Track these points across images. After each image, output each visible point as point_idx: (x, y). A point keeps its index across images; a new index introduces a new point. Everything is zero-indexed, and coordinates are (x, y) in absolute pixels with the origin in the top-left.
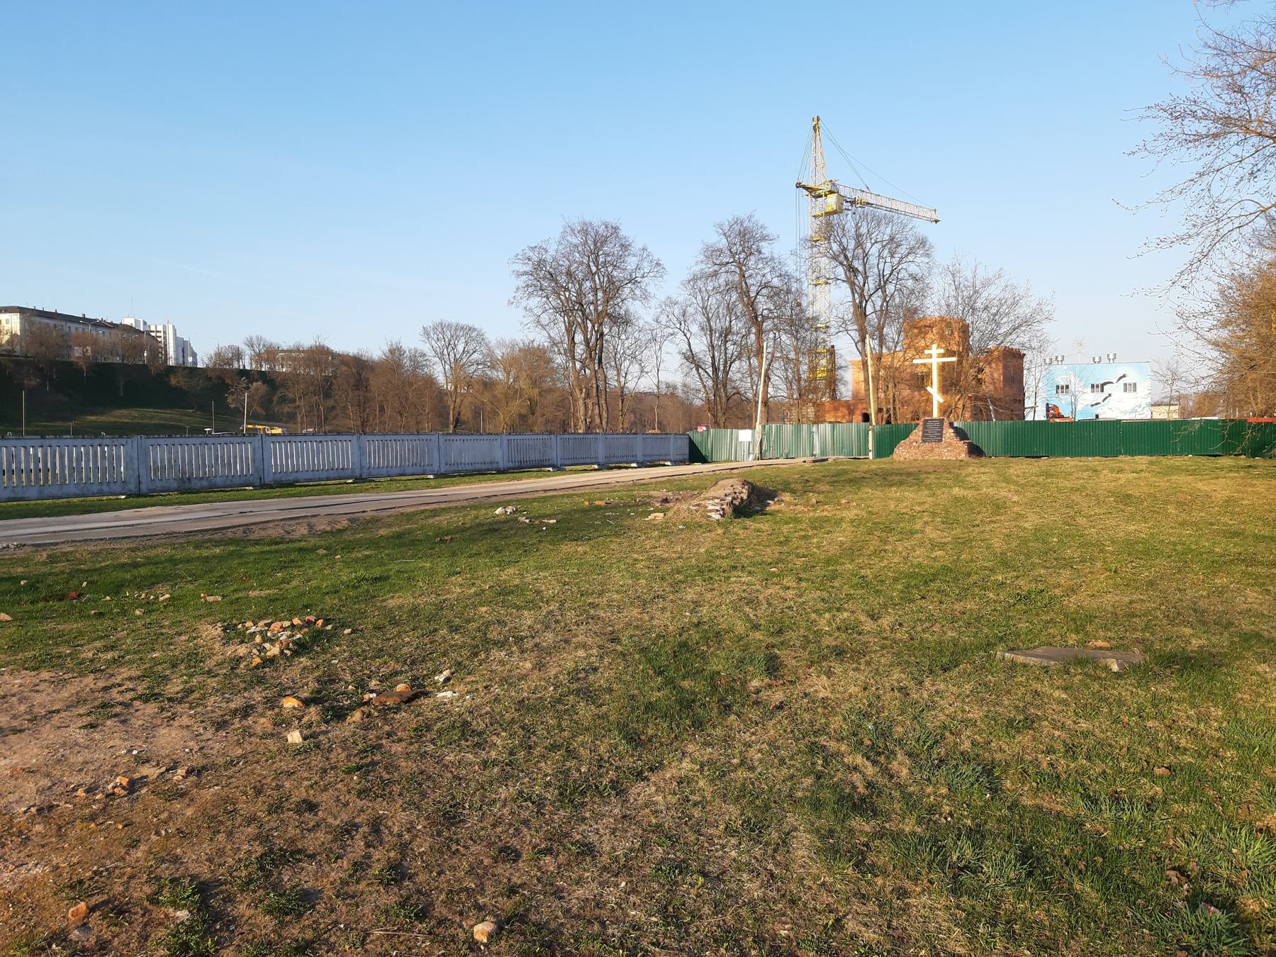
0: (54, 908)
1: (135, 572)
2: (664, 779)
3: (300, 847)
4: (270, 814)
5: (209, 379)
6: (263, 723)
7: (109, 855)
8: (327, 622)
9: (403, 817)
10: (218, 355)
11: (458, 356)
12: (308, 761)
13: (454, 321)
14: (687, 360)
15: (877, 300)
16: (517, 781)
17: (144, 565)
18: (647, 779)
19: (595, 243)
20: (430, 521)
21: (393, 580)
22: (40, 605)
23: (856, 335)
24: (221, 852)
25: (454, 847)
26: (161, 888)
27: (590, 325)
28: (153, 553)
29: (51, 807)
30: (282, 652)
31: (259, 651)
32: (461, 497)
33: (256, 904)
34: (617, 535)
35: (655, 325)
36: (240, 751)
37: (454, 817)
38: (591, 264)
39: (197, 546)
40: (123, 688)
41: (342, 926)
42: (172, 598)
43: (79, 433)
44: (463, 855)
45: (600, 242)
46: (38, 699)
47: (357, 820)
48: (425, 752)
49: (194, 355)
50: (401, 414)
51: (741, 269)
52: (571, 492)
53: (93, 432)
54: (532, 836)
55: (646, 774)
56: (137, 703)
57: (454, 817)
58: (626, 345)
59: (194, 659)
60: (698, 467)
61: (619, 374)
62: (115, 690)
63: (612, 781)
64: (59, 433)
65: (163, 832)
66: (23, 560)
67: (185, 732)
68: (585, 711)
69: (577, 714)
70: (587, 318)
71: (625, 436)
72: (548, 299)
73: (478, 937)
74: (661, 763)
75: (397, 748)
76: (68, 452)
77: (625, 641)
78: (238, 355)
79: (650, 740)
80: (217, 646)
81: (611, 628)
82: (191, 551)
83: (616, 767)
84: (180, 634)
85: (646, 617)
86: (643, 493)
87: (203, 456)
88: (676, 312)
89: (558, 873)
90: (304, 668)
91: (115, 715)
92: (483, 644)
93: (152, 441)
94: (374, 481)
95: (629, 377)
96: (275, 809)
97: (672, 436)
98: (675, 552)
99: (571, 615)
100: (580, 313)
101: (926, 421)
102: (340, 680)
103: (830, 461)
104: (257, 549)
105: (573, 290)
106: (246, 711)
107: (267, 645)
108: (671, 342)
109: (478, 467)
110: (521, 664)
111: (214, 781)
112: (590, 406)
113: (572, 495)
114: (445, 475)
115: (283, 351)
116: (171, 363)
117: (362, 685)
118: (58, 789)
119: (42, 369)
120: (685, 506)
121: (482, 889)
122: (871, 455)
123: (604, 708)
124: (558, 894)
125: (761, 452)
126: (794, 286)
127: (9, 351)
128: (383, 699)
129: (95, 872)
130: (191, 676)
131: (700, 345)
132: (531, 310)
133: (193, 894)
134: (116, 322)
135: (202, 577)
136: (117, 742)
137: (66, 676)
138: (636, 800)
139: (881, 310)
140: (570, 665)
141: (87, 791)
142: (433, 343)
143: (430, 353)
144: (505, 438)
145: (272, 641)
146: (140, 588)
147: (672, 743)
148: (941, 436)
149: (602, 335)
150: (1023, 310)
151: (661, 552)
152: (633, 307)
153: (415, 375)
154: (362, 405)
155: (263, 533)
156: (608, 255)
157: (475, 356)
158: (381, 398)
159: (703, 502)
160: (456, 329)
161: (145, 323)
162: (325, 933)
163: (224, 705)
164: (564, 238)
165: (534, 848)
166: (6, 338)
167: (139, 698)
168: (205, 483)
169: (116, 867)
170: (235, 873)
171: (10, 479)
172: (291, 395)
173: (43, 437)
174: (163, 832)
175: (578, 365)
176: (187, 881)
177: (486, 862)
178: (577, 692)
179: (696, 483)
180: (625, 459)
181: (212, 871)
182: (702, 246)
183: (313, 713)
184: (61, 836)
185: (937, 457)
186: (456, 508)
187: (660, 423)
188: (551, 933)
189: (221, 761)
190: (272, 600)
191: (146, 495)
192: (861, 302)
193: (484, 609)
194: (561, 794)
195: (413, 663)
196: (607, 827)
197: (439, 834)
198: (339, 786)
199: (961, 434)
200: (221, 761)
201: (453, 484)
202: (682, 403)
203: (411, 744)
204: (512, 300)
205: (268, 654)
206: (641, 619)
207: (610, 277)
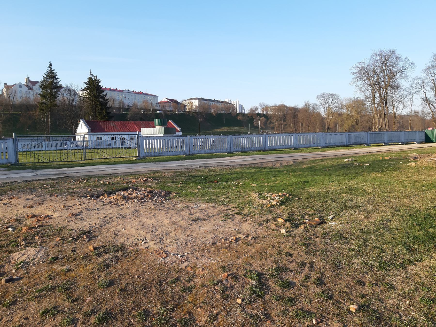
0: (218, 273)
1: (232, 176)
2: (423, 266)
3: (288, 267)
4: (277, 255)
5: (249, 117)
6: (273, 226)
7: (232, 260)
8: (290, 195)
10: (251, 109)
11: (329, 105)
12: (288, 240)
13: (328, 93)
14: (424, 101)
16: (362, 258)
17: (234, 174)
18: (415, 264)
19: (385, 58)
20: (321, 163)
21: (310, 183)
22: (208, 184)
24: (264, 264)
26: (247, 272)
27: (382, 90)
28: (236, 170)
29: (215, 243)
30: (277, 204)
31: (270, 203)
32: (331, 155)
33: (275, 283)
34: (395, 170)
35: (410, 88)
36: (266, 234)
37: (339, 266)
38: (383, 66)
39: (248, 169)
40: (232, 210)
41: (303, 296)
42: (242, 184)
43: (214, 134)
44: (343, 280)
45: (387, 58)
46: (210, 211)
47: (305, 262)
48: (327, 242)
49: (244, 110)
50: (308, 126)
52: (374, 154)
53: (218, 134)
54: (369, 278)
55: (415, 262)
56: (236, 215)
57: (339, 266)
58: (397, 97)
59: (250, 203)
60: (429, 144)
61: (394, 108)
62: (229, 211)
63: (400, 263)
64: (209, 134)
65: (246, 255)
66: (202, 171)
67: (250, 226)
68: (388, 236)
69: (384, 236)
70: (381, 87)
71: (396, 132)
72: (365, 81)
73: (351, 309)
74: (421, 259)
75: (317, 240)
77: (402, 211)
78: (257, 109)
80: (257, 200)
81: (396, 206)
82: (246, 170)
83: (402, 258)
84: (246, 195)
85: (411, 203)
86: (405, 155)
87: (248, 141)
89: (381, 293)
90: (284, 209)
91: (230, 218)
92: (344, 207)
93: (234, 136)
95: (398, 109)
96: (279, 253)
97: (417, 132)
98: (422, 178)
99: (378, 200)
100: (378, 85)
102: (296, 214)
104: (265, 170)
105: (376, 77)
106: (267, 221)
107: (272, 201)
108: (417, 94)
109: (337, 144)
110: (360, 216)
111: (260, 242)
112: (381, 121)
113: (375, 155)
114: (325, 147)
115: (270, 107)
116: (238, 112)
117: (303, 217)
118: (217, 238)
119: (204, 116)
120: (425, 160)
121: (351, 293)
123: (396, 236)
124: (381, 300)
127: (195, 111)
128: (310, 222)
129: (228, 264)
130: (250, 208)
132: (358, 86)
133: (257, 276)
134: (223, 101)
135: (250, 178)
136: (232, 226)
137: (216, 205)
138: (411, 272)
140: (380, 218)
141: (225, 240)
144: (347, 134)
145: (273, 200)
146: (233, 181)
147: (425, 252)
149: (387, 93)
151: (415, 178)
153: (314, 113)
155: (266, 165)
156: (390, 62)
158: (302, 121)
159: (434, 159)
160: (329, 95)
161: (231, 101)
162: (298, 297)
163: (260, 218)
164: (372, 58)
165: (370, 282)
166: (195, 107)
167: (236, 213)
168: (249, 149)
169: (234, 264)
170: (268, 272)
171: (197, 148)
172: (273, 121)
173: (206, 136)
174: (246, 255)
175: (376, 105)
176: (254, 272)
177: (352, 284)
178: (384, 228)
179: (429, 151)
180: (396, 141)
181: (262, 270)
182: (432, 55)
183: (288, 224)
184: (219, 252)
186: (330, 159)
187: (411, 127)
188: (379, 314)
189: (261, 236)
190: (272, 187)
191: (232, 153)
193: (344, 195)
194: (380, 265)
195: (320, 211)
196: (399, 280)
197: (334, 271)
198: (299, 249)
200: (261, 236)
201: (328, 150)
202: (422, 119)
203: (322, 239)
205: (272, 204)
206: (409, 203)
207: (391, 71)
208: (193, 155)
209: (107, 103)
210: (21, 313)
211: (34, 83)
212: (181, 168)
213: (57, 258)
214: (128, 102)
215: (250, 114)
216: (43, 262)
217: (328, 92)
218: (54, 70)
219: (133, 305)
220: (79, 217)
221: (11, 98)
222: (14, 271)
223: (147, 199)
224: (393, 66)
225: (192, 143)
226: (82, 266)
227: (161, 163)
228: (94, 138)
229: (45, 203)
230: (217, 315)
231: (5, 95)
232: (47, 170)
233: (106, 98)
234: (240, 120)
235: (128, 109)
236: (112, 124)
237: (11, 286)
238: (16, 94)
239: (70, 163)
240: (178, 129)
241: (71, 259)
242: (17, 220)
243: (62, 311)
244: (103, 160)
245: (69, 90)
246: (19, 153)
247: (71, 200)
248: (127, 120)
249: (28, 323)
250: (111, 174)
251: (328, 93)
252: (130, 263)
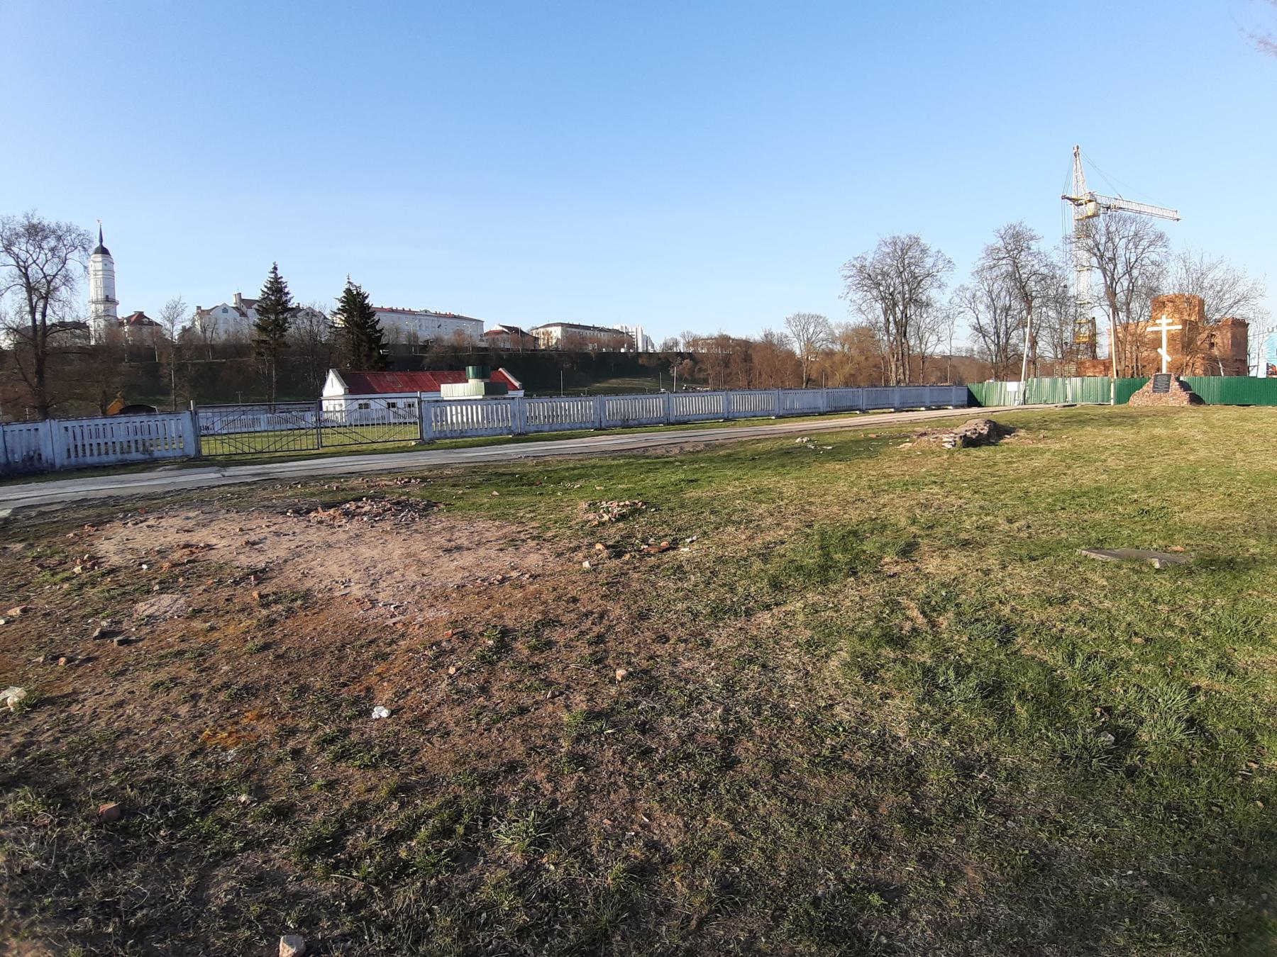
5: (660, 359)
9: (618, 611)
10: (665, 344)
19: (902, 250)
24: (522, 617)
25: (636, 631)
30: (610, 519)
39: (613, 460)
49: (653, 346)
51: (1014, 262)
61: (921, 343)
78: (676, 344)
79: (787, 588)
87: (635, 406)
88: (968, 296)
93: (607, 398)
95: (929, 345)
103: (1078, 406)
109: (805, 411)
116: (640, 350)
122: (1112, 402)
126: (1058, 273)
130: (560, 528)
131: (986, 319)
134: (611, 328)
143: (791, 335)
150: (1241, 288)
154: (748, 372)
157: (821, 335)
166: (554, 341)
168: (636, 422)
172: (704, 367)
180: (915, 405)
193: (738, 502)
194: (712, 611)
199: (1184, 386)
208: (526, 434)
209: (380, 337)
210: (127, 685)
211: (249, 303)
212: (488, 459)
213: (201, 611)
214: (425, 335)
215: (662, 353)
216: (179, 617)
217: (805, 311)
218: (281, 277)
219: (288, 678)
220: (256, 547)
221: (208, 334)
222: (134, 629)
223: (388, 515)
224: (917, 266)
225: (524, 413)
226: (234, 623)
227: (457, 451)
228: (356, 405)
229: (213, 524)
230: (409, 690)
231: (198, 327)
232: (244, 468)
233: (378, 327)
234: (643, 366)
235: (425, 347)
236: (389, 378)
237: (125, 650)
238: (216, 326)
239: (297, 453)
240: (517, 384)
241: (220, 613)
242: (159, 552)
243: (182, 683)
244: (354, 448)
245: (311, 314)
246: (203, 438)
247: (256, 518)
248: (422, 369)
249: (132, 698)
250: (353, 473)
252: (308, 618)
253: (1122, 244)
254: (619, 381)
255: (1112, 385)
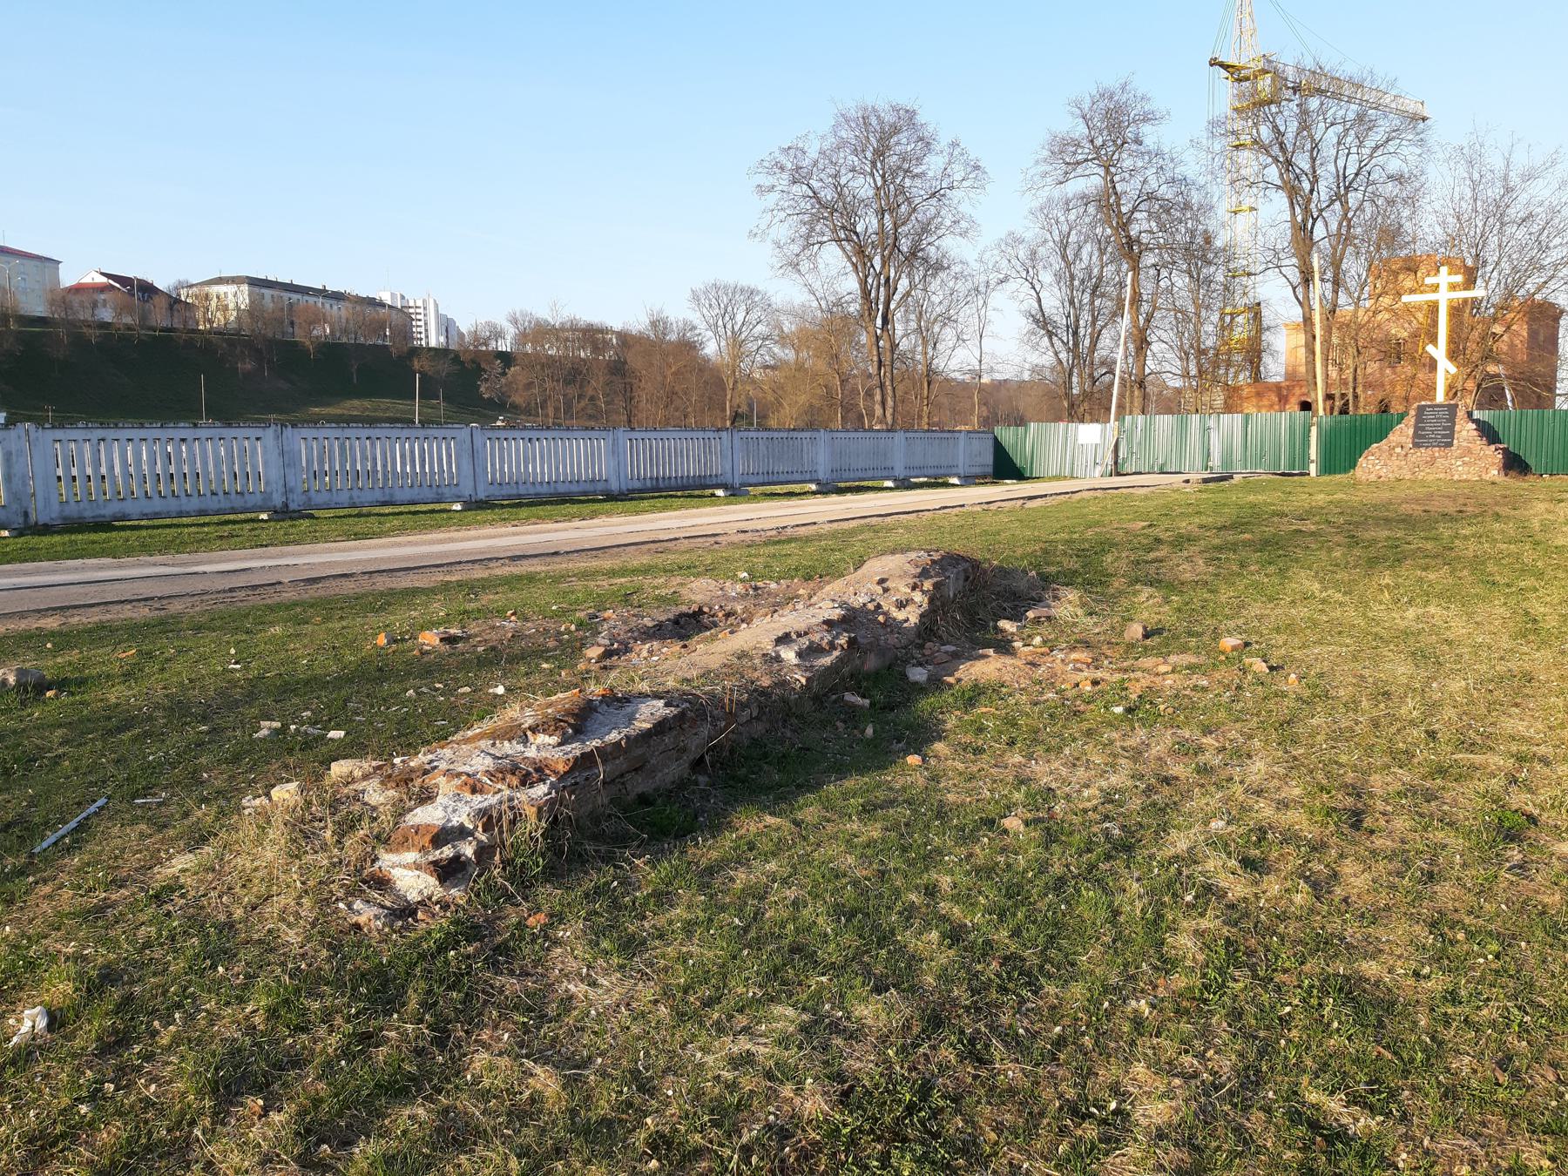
11: (736, 329)
13: (731, 281)
15: (1333, 217)
23: (1295, 276)
45: (886, 136)
60: (1010, 489)
76: (214, 452)
78: (498, 334)
88: (1022, 255)
94: (312, 517)
101: (1421, 409)
109: (562, 489)
122: (1313, 469)
125: (1116, 463)
126: (1195, 198)
131: (1053, 302)
139: (1339, 234)
142: (705, 311)
148: (1452, 436)
152: (949, 245)
157: (759, 327)
160: (734, 293)
161: (403, 297)
180: (870, 474)
185: (1442, 476)
192: (1305, 221)
199: (1488, 433)
204: (755, 230)
251: (733, 286)
253: (1331, 136)
254: (367, 403)
255: (1314, 430)
